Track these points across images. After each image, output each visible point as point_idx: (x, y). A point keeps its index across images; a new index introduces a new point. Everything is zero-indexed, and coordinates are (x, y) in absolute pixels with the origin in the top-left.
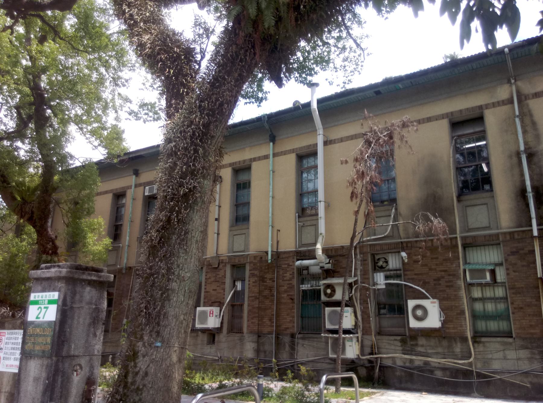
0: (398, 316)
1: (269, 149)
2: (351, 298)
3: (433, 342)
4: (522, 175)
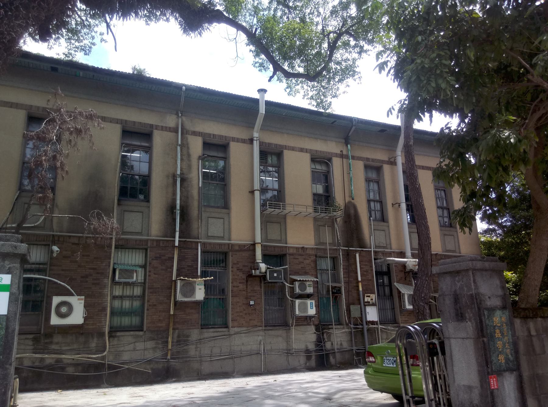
0: (32, 313)
4: (174, 194)
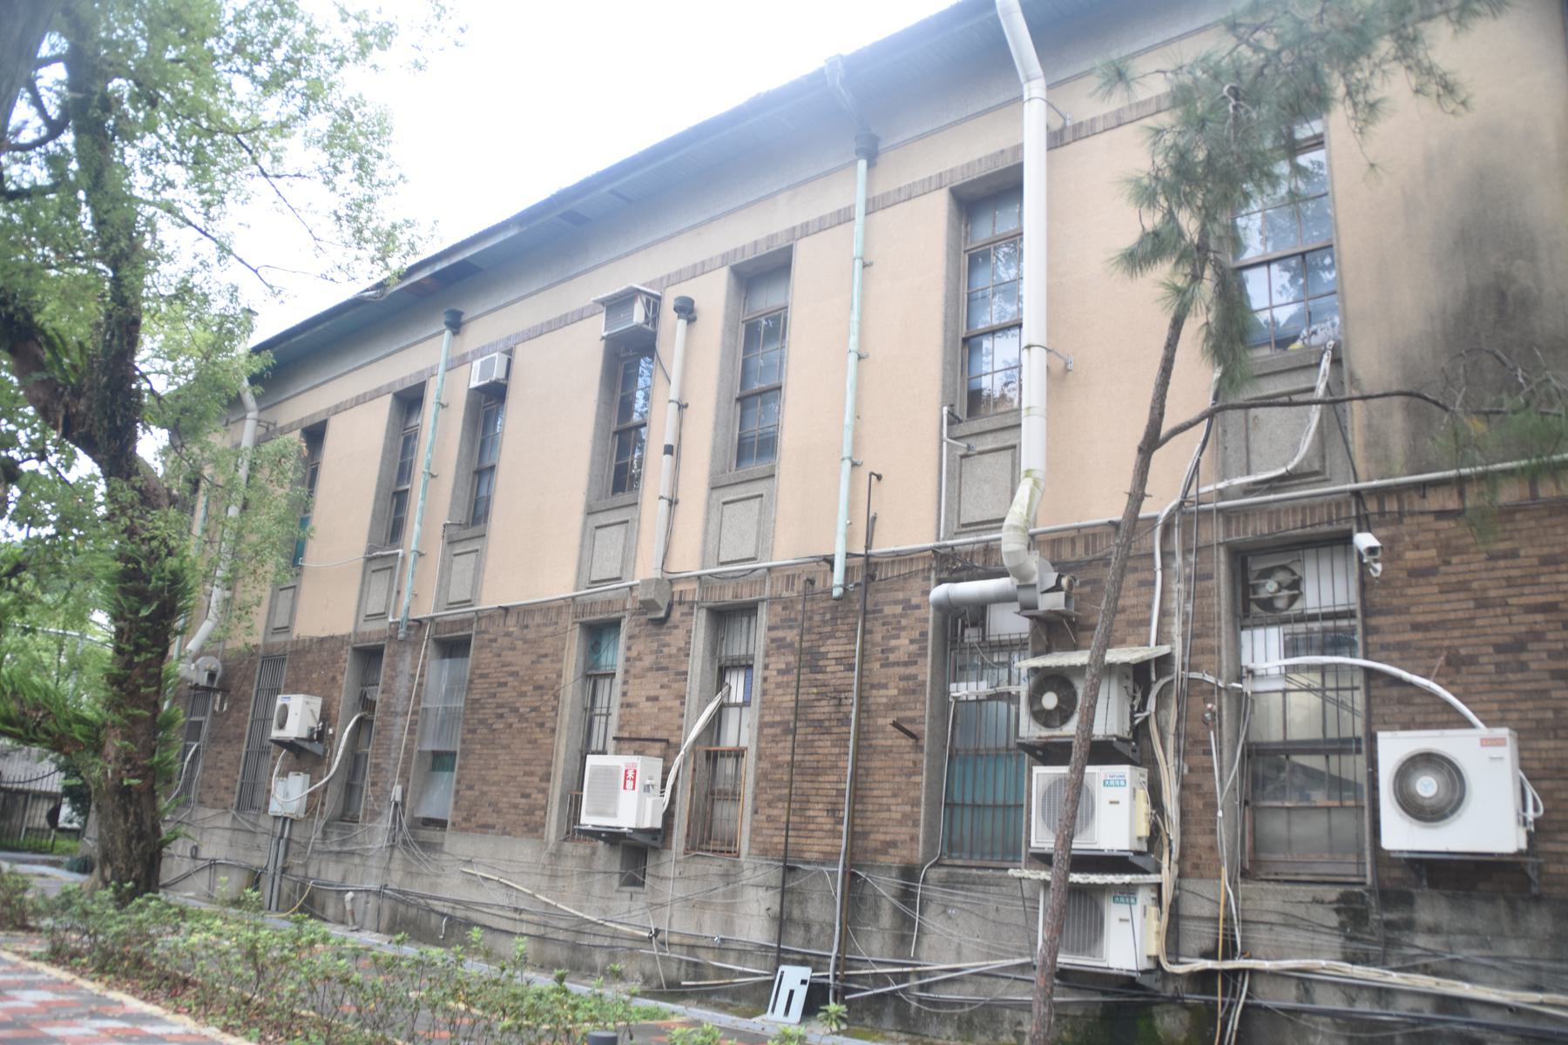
1: (854, 188)
2: (1140, 731)
3: (1482, 917)
